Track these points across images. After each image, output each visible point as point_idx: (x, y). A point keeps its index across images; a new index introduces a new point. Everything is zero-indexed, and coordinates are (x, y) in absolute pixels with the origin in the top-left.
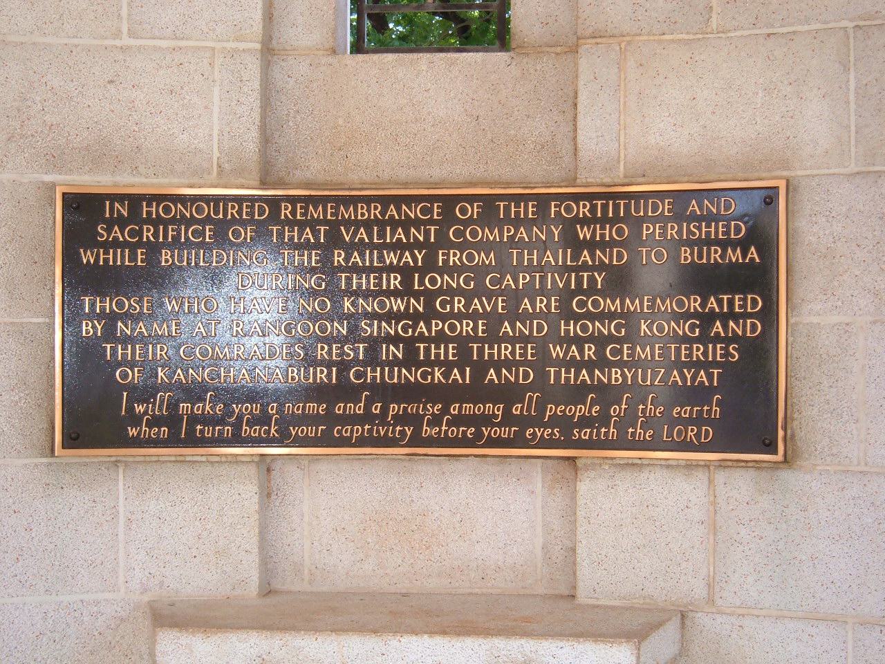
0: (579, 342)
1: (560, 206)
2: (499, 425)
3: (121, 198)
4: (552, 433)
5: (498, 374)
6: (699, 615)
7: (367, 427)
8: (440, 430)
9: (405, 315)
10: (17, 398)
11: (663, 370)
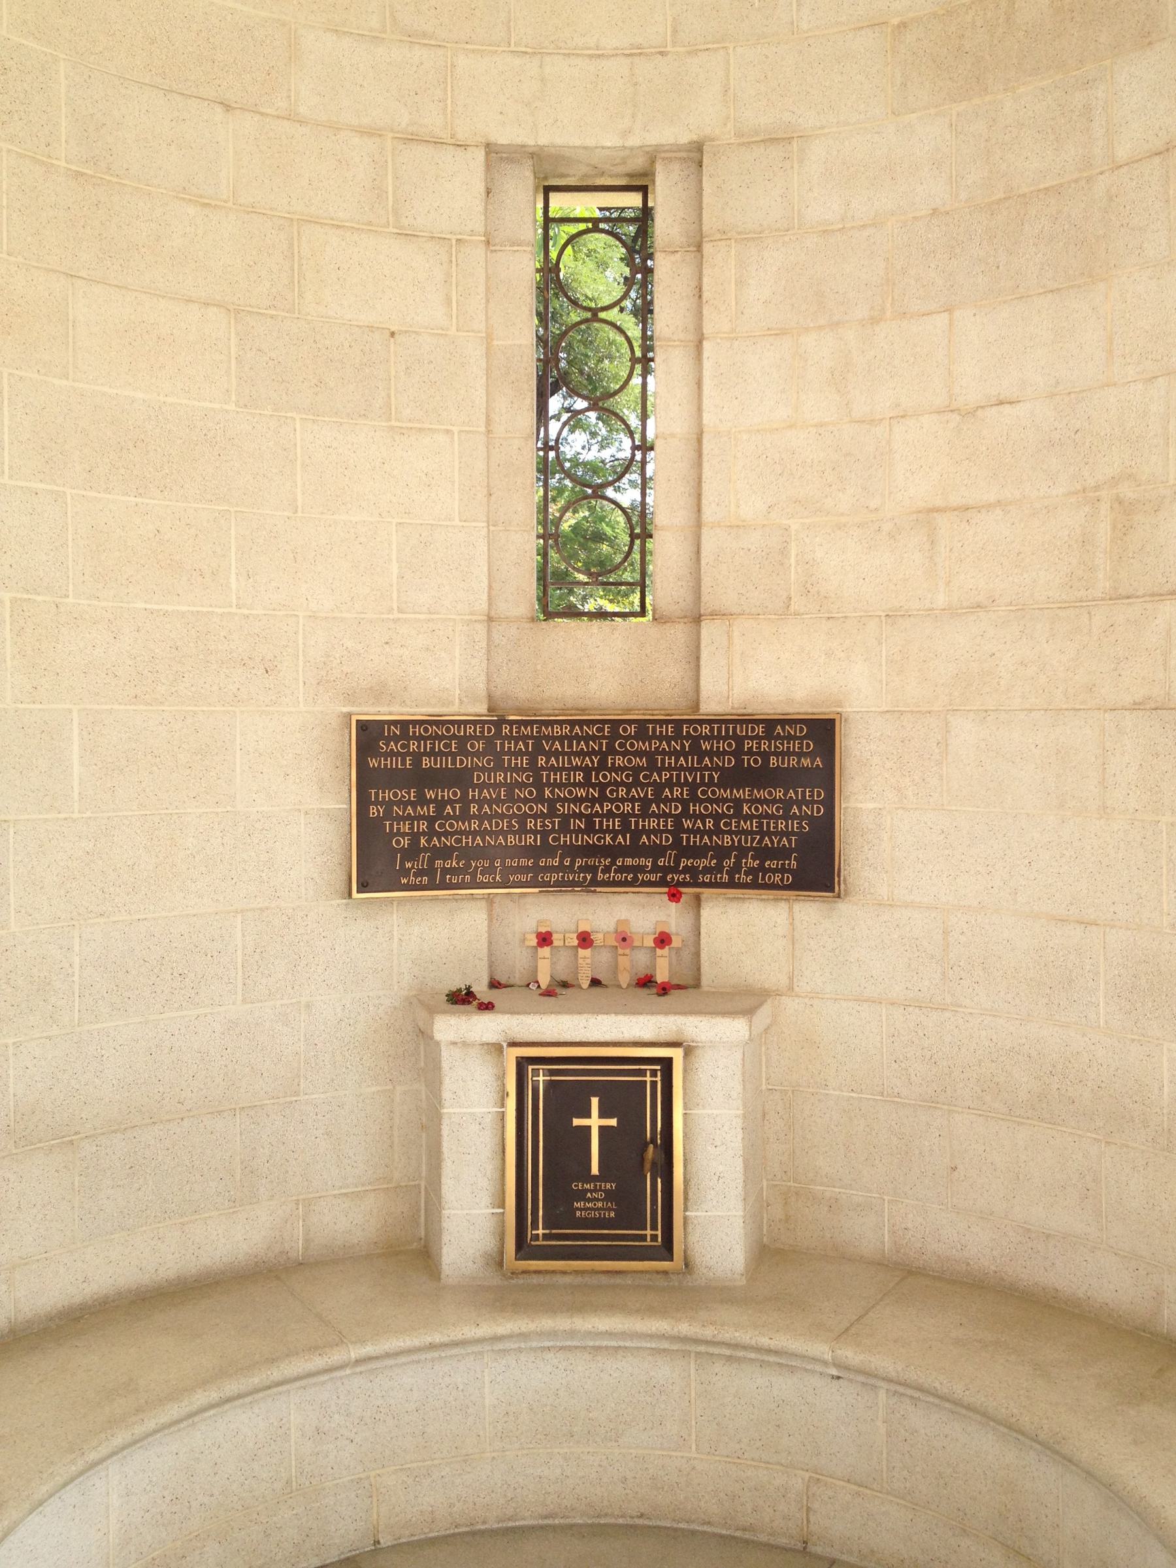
0: (703, 818)
1: (689, 728)
2: (650, 872)
3: (395, 723)
4: (685, 878)
5: (649, 839)
6: (784, 997)
7: (560, 874)
8: (610, 877)
9: (586, 799)
10: (326, 860)
11: (758, 837)
